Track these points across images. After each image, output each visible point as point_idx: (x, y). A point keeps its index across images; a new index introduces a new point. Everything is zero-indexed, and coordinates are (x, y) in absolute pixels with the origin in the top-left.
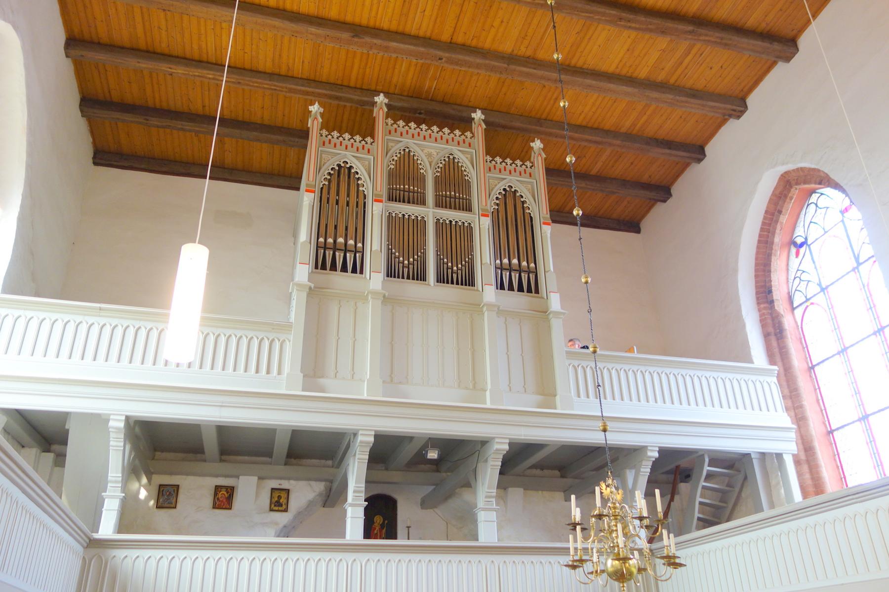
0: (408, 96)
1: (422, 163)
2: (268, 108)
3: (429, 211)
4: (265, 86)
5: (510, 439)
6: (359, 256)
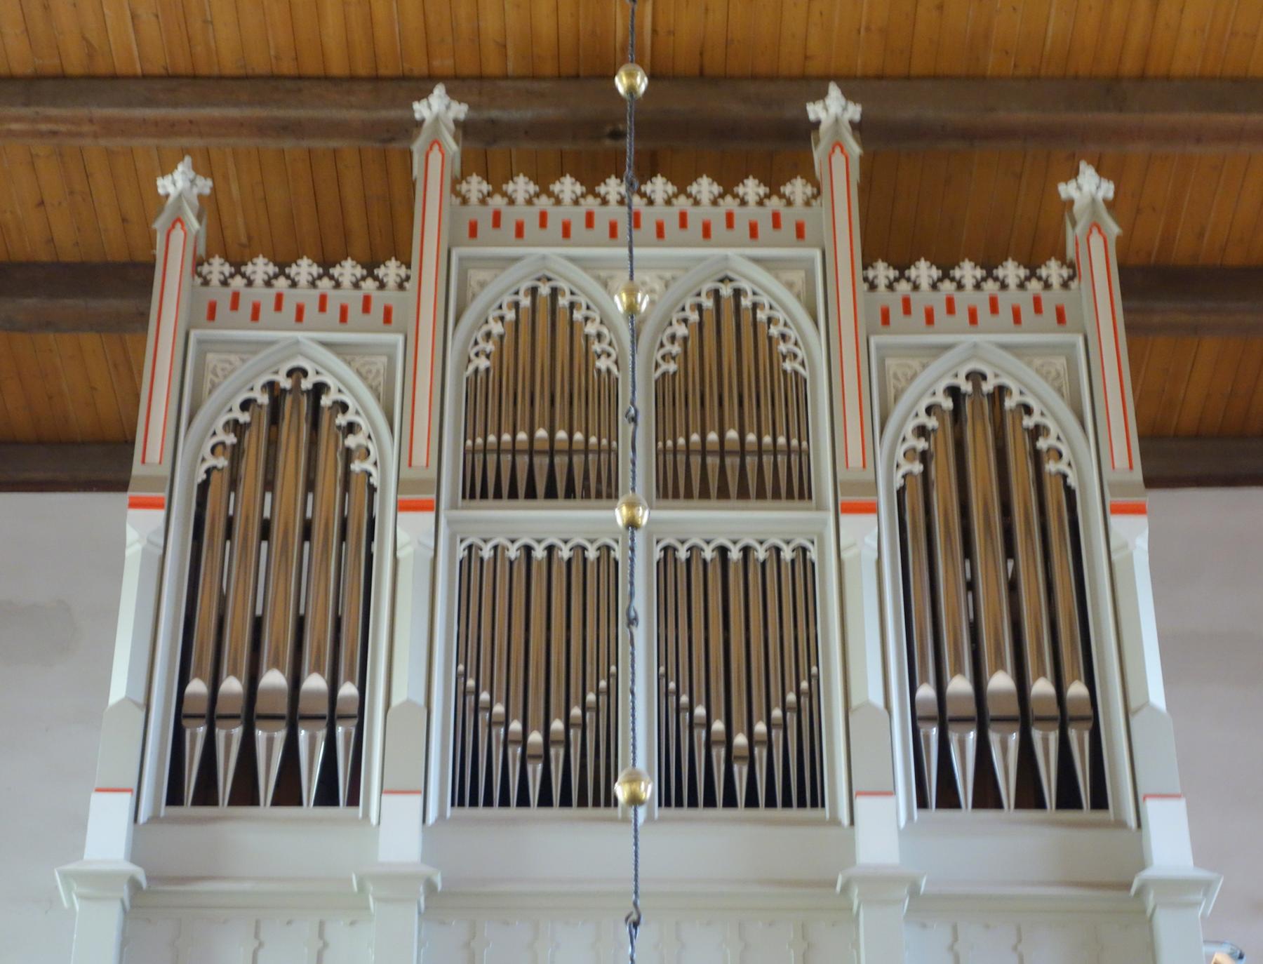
0: (559, 77)
1: (605, 331)
2: (60, 203)
4: (15, 126)
6: (347, 735)
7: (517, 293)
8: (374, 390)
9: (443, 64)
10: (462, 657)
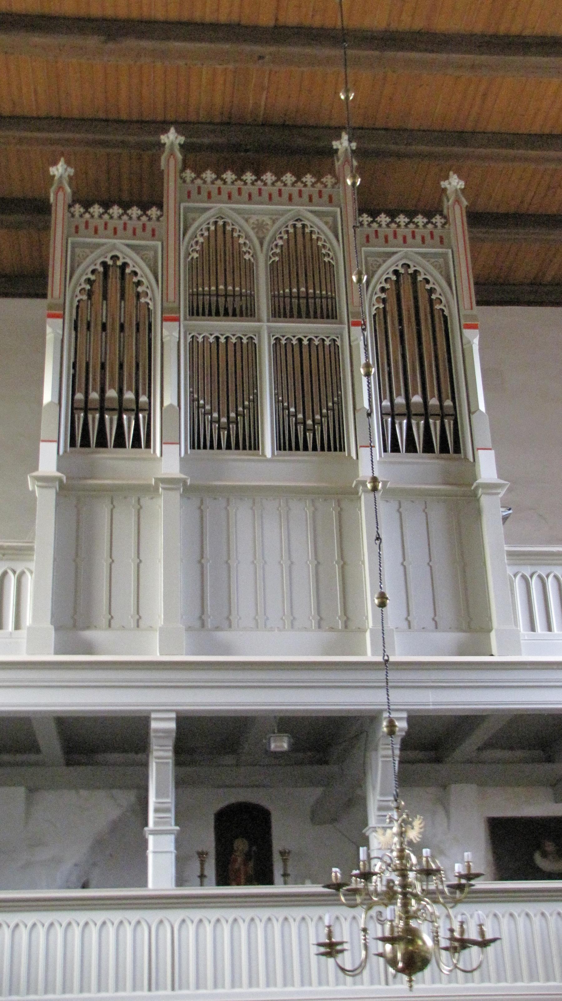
1: (247, 242)
3: (260, 327)
5: (408, 711)
6: (144, 417)
7: (208, 224)
8: (149, 266)
9: (171, 116)
10: (191, 385)
